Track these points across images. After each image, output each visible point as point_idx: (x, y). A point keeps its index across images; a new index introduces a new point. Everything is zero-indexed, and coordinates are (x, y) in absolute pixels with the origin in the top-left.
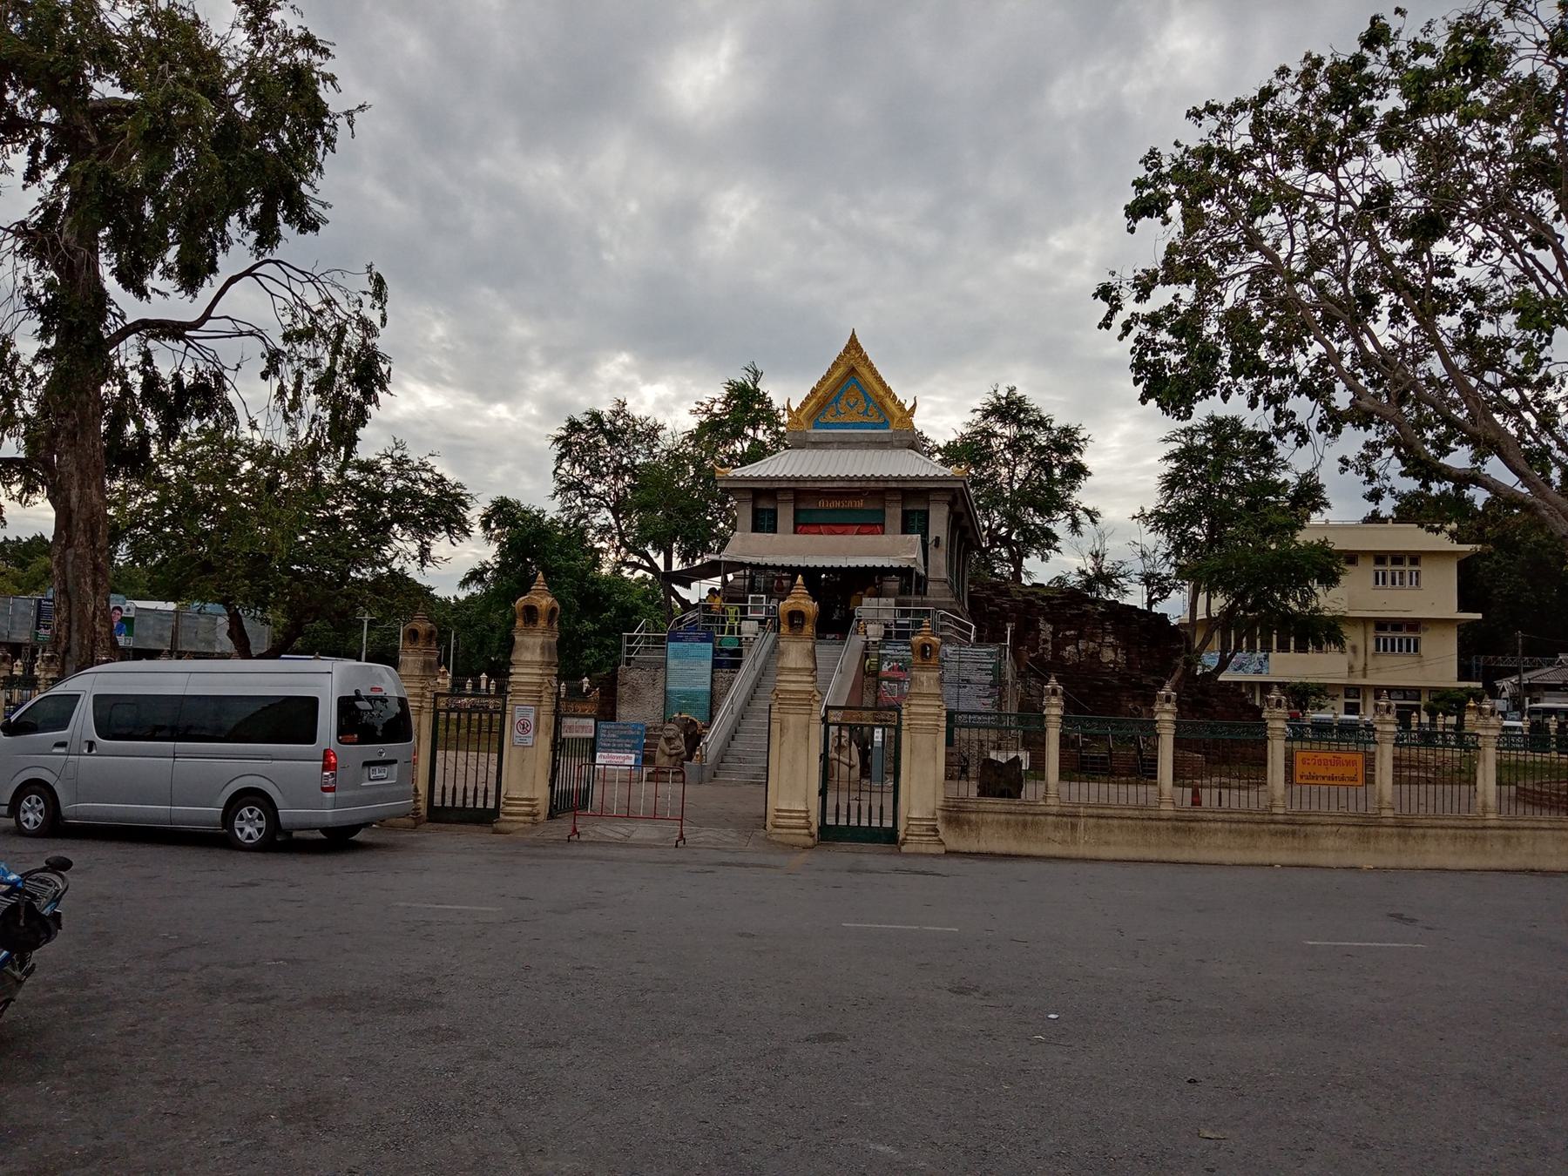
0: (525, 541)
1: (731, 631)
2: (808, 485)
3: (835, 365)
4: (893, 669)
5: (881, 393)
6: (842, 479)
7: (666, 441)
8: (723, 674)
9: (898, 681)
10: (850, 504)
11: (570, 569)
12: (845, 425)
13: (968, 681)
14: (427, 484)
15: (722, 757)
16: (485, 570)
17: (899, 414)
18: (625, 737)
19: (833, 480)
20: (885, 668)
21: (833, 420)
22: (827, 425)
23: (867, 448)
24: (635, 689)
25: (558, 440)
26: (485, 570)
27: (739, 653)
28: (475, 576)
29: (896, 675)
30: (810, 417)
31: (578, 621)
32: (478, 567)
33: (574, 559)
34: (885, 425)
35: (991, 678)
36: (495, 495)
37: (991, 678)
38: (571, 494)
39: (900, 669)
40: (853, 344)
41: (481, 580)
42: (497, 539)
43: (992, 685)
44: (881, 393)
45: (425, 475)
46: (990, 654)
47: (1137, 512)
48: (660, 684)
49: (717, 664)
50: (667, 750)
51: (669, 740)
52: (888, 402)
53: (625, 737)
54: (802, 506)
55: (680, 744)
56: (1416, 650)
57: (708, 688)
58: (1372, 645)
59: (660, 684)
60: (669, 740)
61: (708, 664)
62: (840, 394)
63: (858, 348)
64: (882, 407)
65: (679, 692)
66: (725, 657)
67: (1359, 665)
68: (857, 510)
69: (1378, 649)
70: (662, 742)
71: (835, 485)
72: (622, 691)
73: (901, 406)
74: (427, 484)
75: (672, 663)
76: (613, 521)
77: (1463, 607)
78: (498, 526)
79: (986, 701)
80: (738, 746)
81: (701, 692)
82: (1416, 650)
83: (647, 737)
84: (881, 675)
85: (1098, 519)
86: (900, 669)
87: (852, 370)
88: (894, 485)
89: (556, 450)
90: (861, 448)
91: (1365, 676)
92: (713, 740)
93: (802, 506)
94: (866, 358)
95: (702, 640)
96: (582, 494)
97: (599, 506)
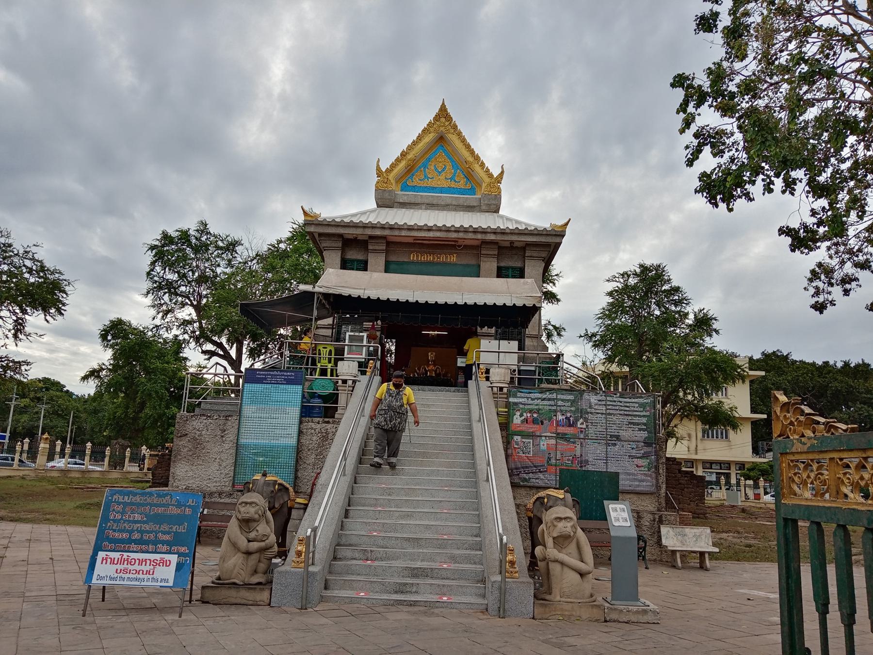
0: (132, 349)
1: (323, 372)
2: (403, 233)
3: (425, 131)
4: (526, 421)
5: (470, 159)
6: (439, 229)
7: (243, 253)
8: (315, 425)
9: (532, 436)
10: (443, 258)
11: (164, 370)
12: (433, 189)
13: (618, 438)
14: (30, 271)
15: (338, 544)
16: (102, 369)
17: (487, 180)
18: (159, 519)
19: (430, 229)
20: (517, 419)
21: (422, 184)
22: (414, 188)
23: (455, 210)
24: (197, 443)
25: (152, 248)
26: (102, 369)
27: (333, 398)
28: (94, 373)
29: (531, 428)
30: (398, 180)
31: (168, 407)
32: (96, 367)
33: (168, 363)
34: (472, 191)
35: (645, 434)
36: (114, 316)
37: (645, 434)
38: (161, 293)
39: (535, 421)
40: (443, 113)
41: (98, 377)
42: (112, 346)
43: (647, 443)
44: (470, 159)
45: (28, 263)
46: (642, 405)
47: (583, 333)
48: (231, 436)
49: (306, 412)
50: (243, 542)
51: (246, 523)
52: (477, 168)
53: (159, 519)
54: (393, 258)
55: (266, 529)
56: (726, 437)
57: (293, 441)
58: (700, 435)
59: (231, 436)
60: (246, 523)
61: (295, 412)
62: (429, 160)
63: (448, 118)
64: (469, 176)
65: (256, 446)
66: (317, 403)
67: (693, 447)
68: (450, 264)
69: (703, 436)
70: (233, 527)
71: (431, 234)
72: (181, 445)
73: (491, 176)
74: (30, 271)
75: (248, 410)
76: (195, 317)
77: (753, 410)
78: (113, 338)
79: (640, 462)
80: (357, 528)
81: (285, 447)
82: (726, 437)
83: (206, 505)
84: (512, 428)
85: (563, 333)
86: (535, 421)
87: (441, 139)
88: (492, 237)
89: (149, 257)
90: (449, 210)
91: (696, 453)
92: (319, 519)
93: (393, 258)
94: (455, 127)
95: (289, 382)
96: (170, 292)
97: (183, 305)
